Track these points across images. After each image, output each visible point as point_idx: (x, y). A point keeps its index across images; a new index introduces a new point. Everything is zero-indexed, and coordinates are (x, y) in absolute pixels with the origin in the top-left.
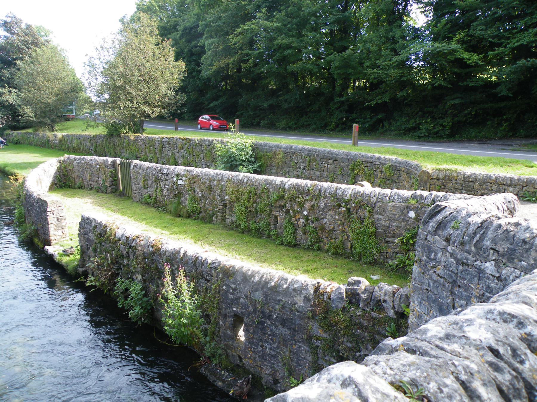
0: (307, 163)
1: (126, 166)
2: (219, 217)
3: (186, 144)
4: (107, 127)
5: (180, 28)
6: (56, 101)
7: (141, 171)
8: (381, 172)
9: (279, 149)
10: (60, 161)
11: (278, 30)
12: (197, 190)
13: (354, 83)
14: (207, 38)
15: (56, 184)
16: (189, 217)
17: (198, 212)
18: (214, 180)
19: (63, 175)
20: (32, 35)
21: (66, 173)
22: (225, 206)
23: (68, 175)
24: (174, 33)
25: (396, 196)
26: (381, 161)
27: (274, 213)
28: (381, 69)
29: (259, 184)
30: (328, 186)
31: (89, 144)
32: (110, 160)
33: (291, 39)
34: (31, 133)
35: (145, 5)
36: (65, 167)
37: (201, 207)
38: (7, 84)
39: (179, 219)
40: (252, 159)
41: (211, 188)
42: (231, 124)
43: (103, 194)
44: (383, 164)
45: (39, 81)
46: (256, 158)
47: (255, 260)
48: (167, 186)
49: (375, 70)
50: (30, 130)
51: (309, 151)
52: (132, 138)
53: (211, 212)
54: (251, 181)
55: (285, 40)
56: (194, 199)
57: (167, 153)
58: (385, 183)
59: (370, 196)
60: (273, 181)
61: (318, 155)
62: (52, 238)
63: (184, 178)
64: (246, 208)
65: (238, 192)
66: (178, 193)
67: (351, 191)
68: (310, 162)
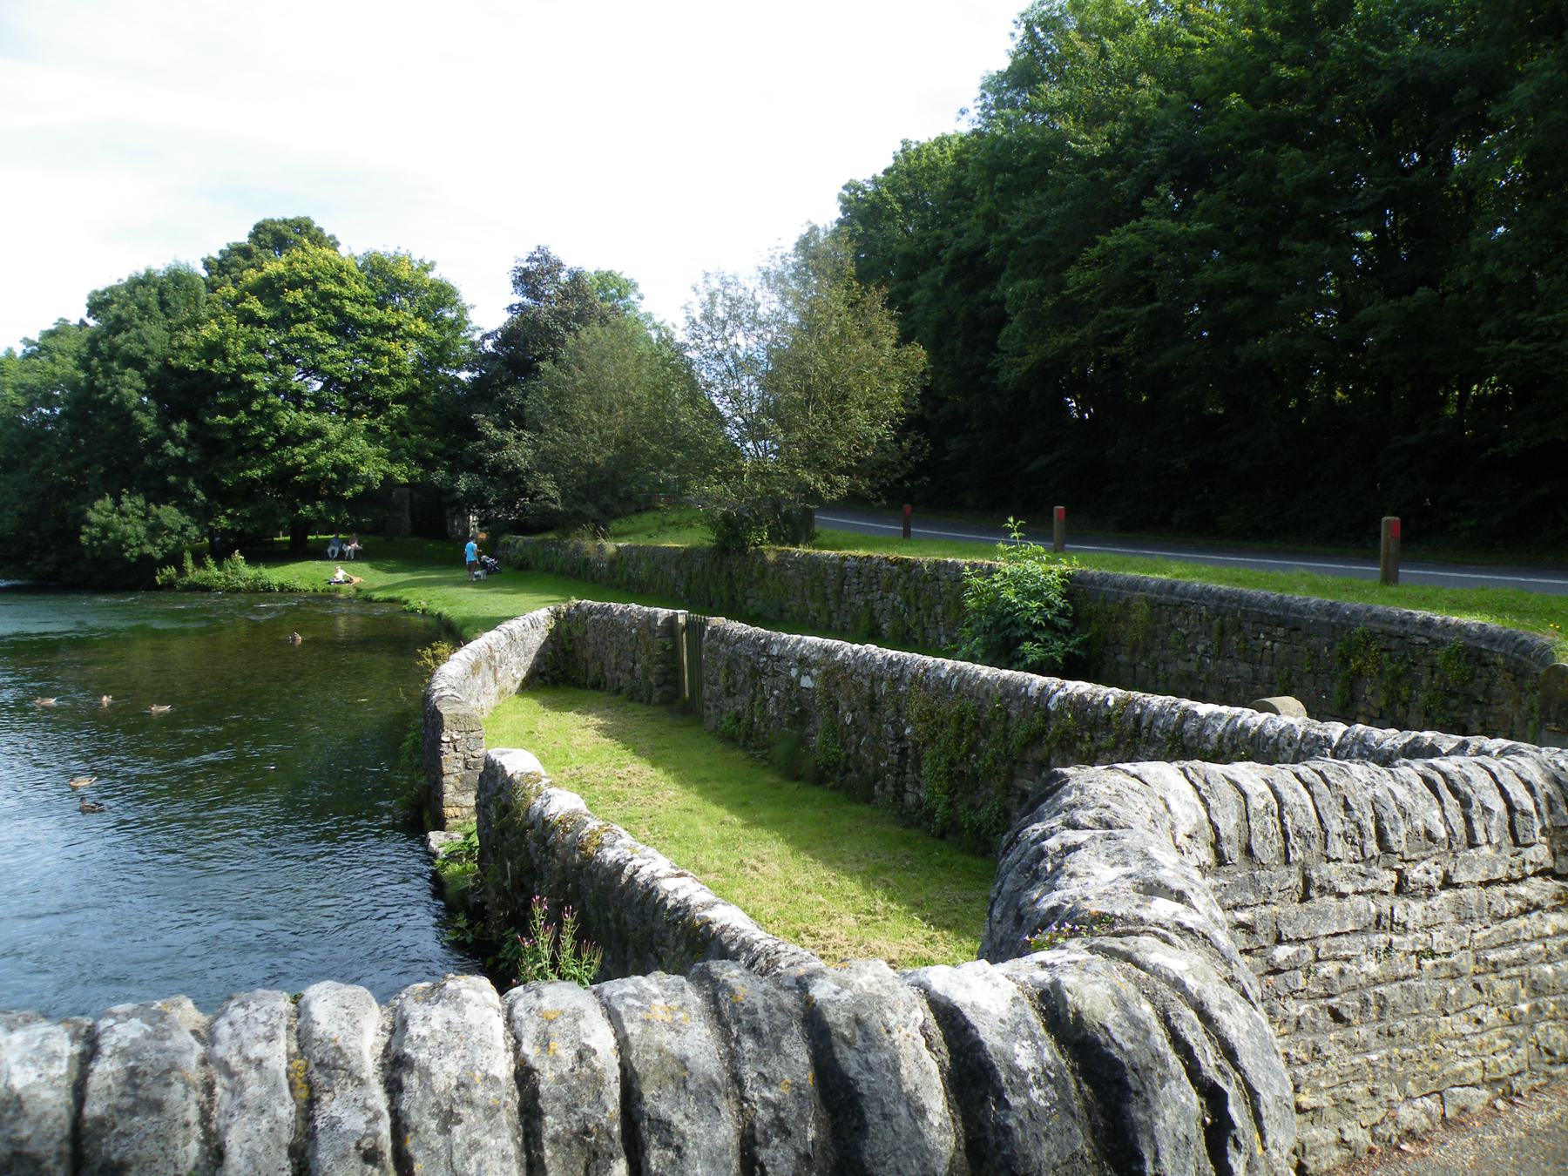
0: (1215, 635)
1: (694, 628)
2: (890, 788)
3: (899, 575)
4: (713, 525)
5: (947, 255)
6: (613, 458)
7: (722, 648)
8: (1433, 668)
9: (1138, 594)
10: (558, 613)
11: (1204, 243)
12: (843, 705)
13: (1465, 390)
14: (1013, 280)
15: (542, 675)
16: (819, 779)
17: (842, 767)
18: (882, 679)
19: (563, 650)
20: (580, 298)
21: (568, 647)
22: (903, 752)
23: (573, 651)
24: (934, 271)
25: (1356, 748)
26: (1431, 632)
27: (1019, 782)
28: (1535, 339)
29: (987, 693)
30: (1162, 708)
31: (673, 572)
32: (663, 613)
33: (1244, 267)
34: (553, 542)
35: (863, 201)
36: (569, 632)
37: (848, 756)
38: (514, 418)
39: (793, 786)
40: (1063, 622)
41: (873, 704)
42: (1011, 520)
43: (639, 706)
44: (1439, 643)
45: (580, 410)
46: (1075, 620)
47: (924, 919)
48: (776, 692)
49: (1514, 344)
50: (551, 536)
51: (1222, 598)
52: (771, 557)
53: (871, 771)
54: (969, 683)
55: (1225, 270)
56: (836, 731)
57: (852, 600)
58: (1445, 705)
59: (1276, 742)
60: (1021, 685)
61: (1245, 613)
62: (449, 812)
63: (814, 672)
64: (951, 763)
65: (933, 717)
66: (800, 711)
67: (1223, 724)
68: (1222, 632)
